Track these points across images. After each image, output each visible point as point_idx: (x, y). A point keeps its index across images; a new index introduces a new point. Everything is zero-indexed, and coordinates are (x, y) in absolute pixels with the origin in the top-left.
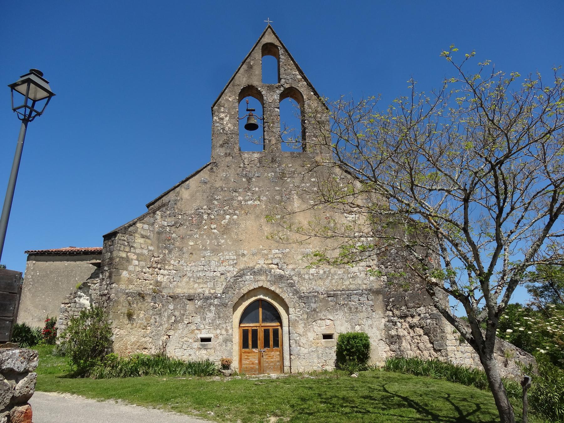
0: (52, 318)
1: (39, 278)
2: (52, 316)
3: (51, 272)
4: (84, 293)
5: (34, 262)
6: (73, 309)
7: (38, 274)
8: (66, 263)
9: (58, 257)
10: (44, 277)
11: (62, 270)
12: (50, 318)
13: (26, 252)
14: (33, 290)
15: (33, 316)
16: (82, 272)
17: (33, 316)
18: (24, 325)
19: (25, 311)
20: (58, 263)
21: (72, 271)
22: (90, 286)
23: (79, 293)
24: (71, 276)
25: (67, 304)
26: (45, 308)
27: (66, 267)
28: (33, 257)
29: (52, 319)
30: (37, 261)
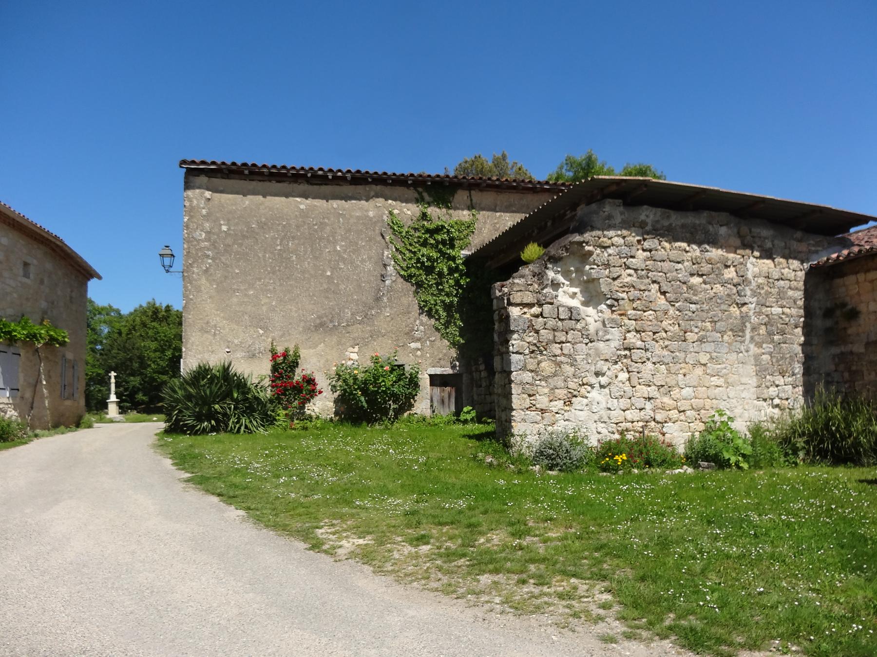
0: (287, 350)
1: (229, 241)
2: (286, 345)
3: (262, 226)
4: (566, 274)
5: (208, 194)
6: (551, 323)
7: (224, 228)
8: (303, 204)
9: (274, 185)
10: (244, 237)
11: (293, 222)
12: (280, 350)
13: (184, 162)
14: (219, 274)
15: (229, 343)
16: (349, 230)
17: (229, 343)
18: (226, 370)
19: (204, 331)
20: (277, 203)
21: (322, 225)
22: (590, 253)
23: (551, 274)
24: (321, 239)
25: (530, 305)
26: (260, 322)
27: (304, 214)
28: (203, 179)
29: (285, 355)
30: (215, 190)
